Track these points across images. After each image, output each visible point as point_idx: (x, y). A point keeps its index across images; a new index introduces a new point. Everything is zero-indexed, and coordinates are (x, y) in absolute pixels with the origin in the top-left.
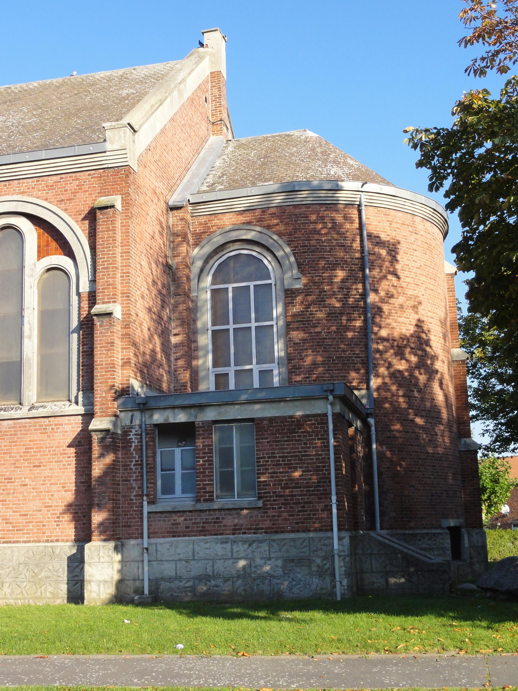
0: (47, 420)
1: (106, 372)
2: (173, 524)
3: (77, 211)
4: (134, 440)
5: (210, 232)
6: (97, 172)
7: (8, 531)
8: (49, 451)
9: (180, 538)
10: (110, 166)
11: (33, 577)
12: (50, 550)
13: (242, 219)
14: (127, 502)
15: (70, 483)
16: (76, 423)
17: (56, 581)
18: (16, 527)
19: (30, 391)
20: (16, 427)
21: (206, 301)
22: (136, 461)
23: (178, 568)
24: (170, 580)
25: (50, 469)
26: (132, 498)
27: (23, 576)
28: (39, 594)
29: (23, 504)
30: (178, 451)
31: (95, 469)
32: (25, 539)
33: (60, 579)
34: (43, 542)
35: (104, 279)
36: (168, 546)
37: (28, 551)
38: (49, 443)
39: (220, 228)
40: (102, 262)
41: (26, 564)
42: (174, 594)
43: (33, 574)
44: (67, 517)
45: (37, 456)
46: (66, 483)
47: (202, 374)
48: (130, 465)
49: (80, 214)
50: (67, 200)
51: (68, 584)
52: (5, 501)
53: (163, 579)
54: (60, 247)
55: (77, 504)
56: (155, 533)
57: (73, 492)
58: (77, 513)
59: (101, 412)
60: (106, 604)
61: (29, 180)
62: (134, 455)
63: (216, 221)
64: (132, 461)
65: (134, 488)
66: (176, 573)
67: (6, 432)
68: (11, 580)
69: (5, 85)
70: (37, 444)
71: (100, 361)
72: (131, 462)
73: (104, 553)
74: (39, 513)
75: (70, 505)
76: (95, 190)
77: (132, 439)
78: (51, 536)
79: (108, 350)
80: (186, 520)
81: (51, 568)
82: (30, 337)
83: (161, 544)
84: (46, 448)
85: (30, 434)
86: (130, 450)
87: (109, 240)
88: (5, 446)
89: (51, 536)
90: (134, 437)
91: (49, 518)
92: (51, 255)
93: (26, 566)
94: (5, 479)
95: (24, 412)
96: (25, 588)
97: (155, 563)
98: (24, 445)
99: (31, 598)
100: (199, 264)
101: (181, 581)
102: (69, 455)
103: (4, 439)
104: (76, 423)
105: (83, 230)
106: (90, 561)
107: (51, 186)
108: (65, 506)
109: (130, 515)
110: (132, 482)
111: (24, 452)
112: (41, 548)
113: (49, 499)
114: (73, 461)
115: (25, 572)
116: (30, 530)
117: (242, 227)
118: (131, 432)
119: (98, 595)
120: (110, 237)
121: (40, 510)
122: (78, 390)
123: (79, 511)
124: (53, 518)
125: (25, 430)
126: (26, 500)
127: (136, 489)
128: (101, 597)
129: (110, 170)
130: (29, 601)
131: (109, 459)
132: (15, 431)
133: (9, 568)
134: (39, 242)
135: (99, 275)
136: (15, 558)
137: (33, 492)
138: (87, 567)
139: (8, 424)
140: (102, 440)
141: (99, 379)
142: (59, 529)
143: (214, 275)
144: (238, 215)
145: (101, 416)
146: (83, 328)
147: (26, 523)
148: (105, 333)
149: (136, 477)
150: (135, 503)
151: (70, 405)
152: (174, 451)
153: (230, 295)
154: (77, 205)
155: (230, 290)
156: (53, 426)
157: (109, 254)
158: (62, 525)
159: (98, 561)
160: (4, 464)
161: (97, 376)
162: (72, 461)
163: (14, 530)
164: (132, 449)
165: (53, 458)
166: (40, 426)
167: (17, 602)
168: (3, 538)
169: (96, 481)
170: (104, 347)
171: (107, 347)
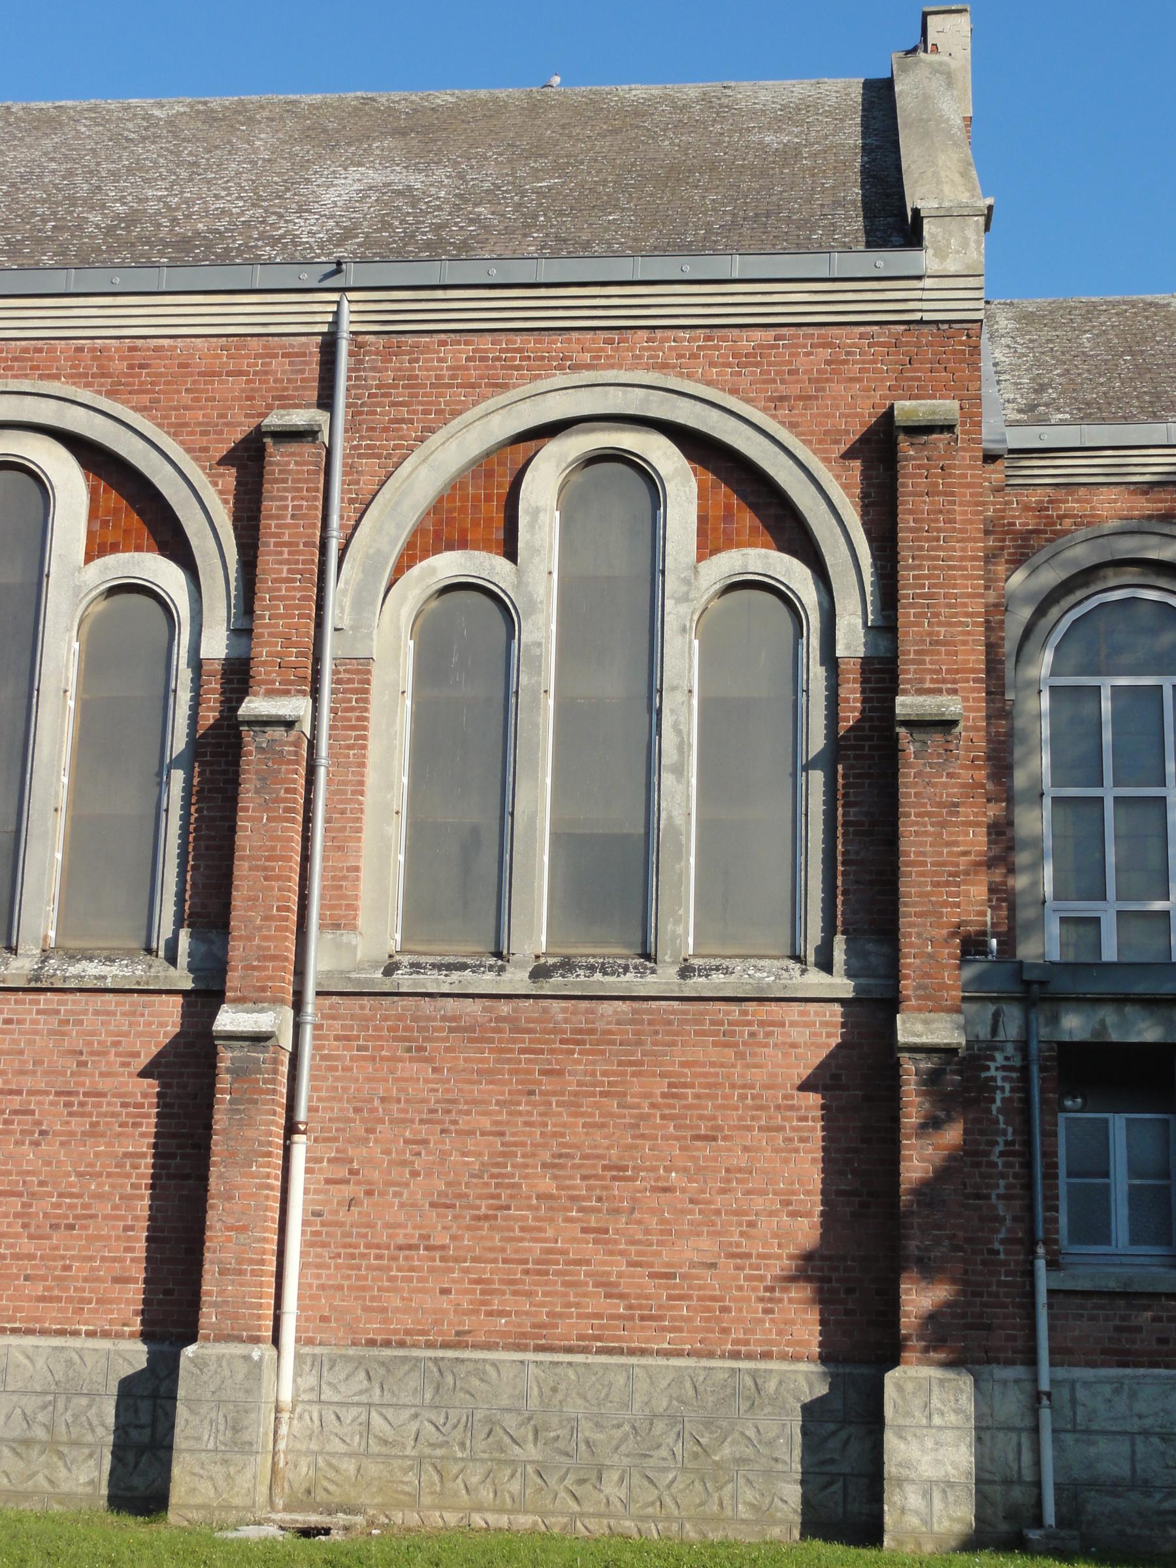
0: (734, 1008)
1: (937, 884)
2: (1118, 1329)
3: (826, 433)
4: (999, 1083)
5: (1054, 532)
6: (886, 329)
7: (612, 1317)
8: (743, 1097)
9: (1142, 1371)
10: (927, 317)
11: (696, 1456)
12: (749, 1382)
13: (1144, 505)
14: (979, 1258)
15: (808, 1193)
16: (824, 1024)
17: (768, 1473)
18: (641, 1307)
19: (677, 922)
20: (641, 1022)
21: (1040, 716)
22: (1007, 1143)
23: (1139, 1456)
24: (1114, 1487)
25: (746, 1149)
26: (997, 1246)
27: (664, 1452)
28: (716, 1508)
29: (660, 1243)
30: (1118, 1123)
31: (910, 1158)
32: (666, 1346)
33: (780, 1467)
34: (722, 1356)
35: (921, 625)
36: (1107, 1390)
37: (678, 1381)
38: (742, 1076)
39: (1082, 524)
40: (915, 577)
41: (674, 1419)
42: (1129, 1530)
43: (696, 1448)
44: (802, 1292)
45: (706, 1108)
46: (793, 1193)
47: (1025, 914)
48: (987, 1154)
49: (837, 442)
50: (799, 398)
51: (803, 1482)
52: (606, 1231)
53: (1093, 1484)
54: (767, 527)
55: (826, 1253)
56: (1069, 1351)
57: (817, 1219)
58: (828, 1280)
59: (919, 998)
60: (954, 1550)
61: (681, 333)
62: (1002, 1126)
63: (1072, 505)
64: (997, 1143)
65: (1002, 1220)
66: (1134, 1470)
67: (610, 1032)
68: (626, 1461)
69: (355, 90)
70: (705, 1075)
71: (917, 854)
72: (994, 1143)
73: (942, 1401)
74: (709, 1273)
75: (808, 1257)
76: (883, 380)
77: (994, 1079)
78: (746, 1343)
79: (943, 824)
80: (1156, 1319)
81: (751, 1433)
82: (679, 770)
83: (1086, 1384)
84: (733, 1086)
85: (684, 1043)
86: (990, 1112)
87: (937, 521)
88: (604, 1073)
89: (746, 1343)
90: (999, 1075)
91: (740, 1288)
92: (739, 545)
93: (673, 1425)
94: (605, 1168)
95: (664, 978)
96: (669, 1486)
97: (1069, 1438)
98: (663, 1075)
99: (689, 1519)
100: (1025, 613)
101: (1148, 1495)
102: (803, 1112)
103: (603, 1052)
104: (823, 1024)
105: (845, 487)
106: (901, 1421)
107: (747, 355)
108: (791, 1257)
109: (990, 1294)
110: (994, 1200)
111: (664, 1095)
112: (723, 1375)
113: (742, 1234)
114: (816, 1131)
115: (670, 1441)
116: (683, 1319)
117: (1147, 526)
118: (993, 1059)
119: (925, 1522)
120: (941, 512)
121: (713, 1265)
122: (179, 923)
123: (834, 1275)
124: (754, 1289)
125: (668, 1033)
126: (669, 1232)
127: (1008, 1223)
128: (936, 1528)
129: (926, 329)
130: (682, 1527)
131: (953, 1135)
132: (635, 1033)
133: (619, 1426)
134: (701, 508)
135: (907, 614)
136: (639, 1399)
137: (691, 1212)
138: (890, 1438)
139: (616, 1012)
140: (932, 1080)
141: (915, 904)
142: (772, 1321)
143: (1057, 649)
144: (1133, 493)
145: (920, 1009)
146: (847, 757)
147: (670, 1298)
148: (932, 775)
149: (1008, 1187)
150: (1005, 1263)
151: (803, 972)
152: (1106, 1121)
153: (1106, 706)
154: (827, 416)
155: (1106, 693)
156: (755, 1028)
157: (937, 558)
158: (781, 1311)
159: (924, 1422)
160: (603, 1125)
161: (909, 895)
162: (813, 1129)
163: (631, 1318)
164: (994, 1108)
165: (753, 1118)
166: (713, 1023)
167: (644, 1526)
168: (599, 1338)
169: (912, 1191)
170: (929, 814)
171: (940, 814)
